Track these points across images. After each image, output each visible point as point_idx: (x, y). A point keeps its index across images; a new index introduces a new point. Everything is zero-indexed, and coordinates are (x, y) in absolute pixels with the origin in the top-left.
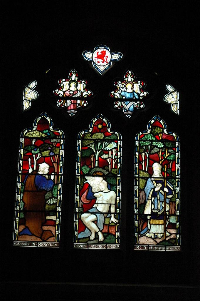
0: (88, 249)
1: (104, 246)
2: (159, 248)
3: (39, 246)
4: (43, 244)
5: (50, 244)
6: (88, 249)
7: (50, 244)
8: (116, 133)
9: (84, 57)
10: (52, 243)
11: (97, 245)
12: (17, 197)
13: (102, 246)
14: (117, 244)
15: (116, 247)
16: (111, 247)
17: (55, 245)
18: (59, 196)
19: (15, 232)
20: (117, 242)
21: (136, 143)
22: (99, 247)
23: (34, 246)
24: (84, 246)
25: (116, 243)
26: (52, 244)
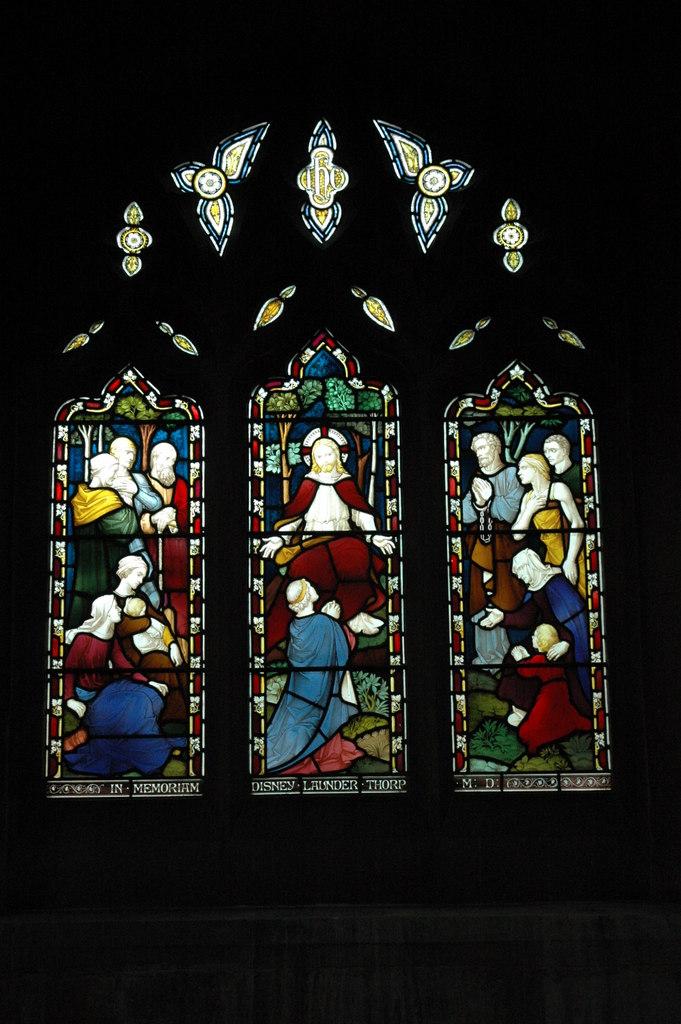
0: (301, 794)
1: (354, 783)
2: (591, 782)
3: (138, 793)
4: (151, 788)
5: (394, 782)
6: (301, 794)
7: (394, 782)
8: (179, 403)
9: (220, 146)
10: (181, 783)
11: (330, 780)
12: (453, 623)
13: (349, 784)
14: (600, 772)
15: (398, 785)
16: (378, 787)
17: (192, 788)
18: (193, 620)
19: (253, 748)
20: (599, 768)
21: (448, 428)
22: (338, 787)
23: (119, 793)
24: (287, 786)
25: (187, 776)
26: (176, 786)
